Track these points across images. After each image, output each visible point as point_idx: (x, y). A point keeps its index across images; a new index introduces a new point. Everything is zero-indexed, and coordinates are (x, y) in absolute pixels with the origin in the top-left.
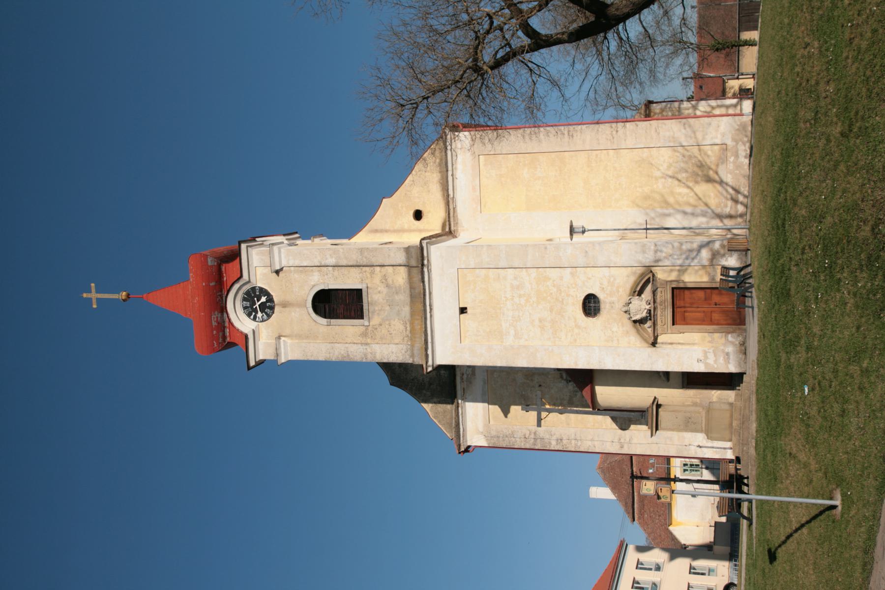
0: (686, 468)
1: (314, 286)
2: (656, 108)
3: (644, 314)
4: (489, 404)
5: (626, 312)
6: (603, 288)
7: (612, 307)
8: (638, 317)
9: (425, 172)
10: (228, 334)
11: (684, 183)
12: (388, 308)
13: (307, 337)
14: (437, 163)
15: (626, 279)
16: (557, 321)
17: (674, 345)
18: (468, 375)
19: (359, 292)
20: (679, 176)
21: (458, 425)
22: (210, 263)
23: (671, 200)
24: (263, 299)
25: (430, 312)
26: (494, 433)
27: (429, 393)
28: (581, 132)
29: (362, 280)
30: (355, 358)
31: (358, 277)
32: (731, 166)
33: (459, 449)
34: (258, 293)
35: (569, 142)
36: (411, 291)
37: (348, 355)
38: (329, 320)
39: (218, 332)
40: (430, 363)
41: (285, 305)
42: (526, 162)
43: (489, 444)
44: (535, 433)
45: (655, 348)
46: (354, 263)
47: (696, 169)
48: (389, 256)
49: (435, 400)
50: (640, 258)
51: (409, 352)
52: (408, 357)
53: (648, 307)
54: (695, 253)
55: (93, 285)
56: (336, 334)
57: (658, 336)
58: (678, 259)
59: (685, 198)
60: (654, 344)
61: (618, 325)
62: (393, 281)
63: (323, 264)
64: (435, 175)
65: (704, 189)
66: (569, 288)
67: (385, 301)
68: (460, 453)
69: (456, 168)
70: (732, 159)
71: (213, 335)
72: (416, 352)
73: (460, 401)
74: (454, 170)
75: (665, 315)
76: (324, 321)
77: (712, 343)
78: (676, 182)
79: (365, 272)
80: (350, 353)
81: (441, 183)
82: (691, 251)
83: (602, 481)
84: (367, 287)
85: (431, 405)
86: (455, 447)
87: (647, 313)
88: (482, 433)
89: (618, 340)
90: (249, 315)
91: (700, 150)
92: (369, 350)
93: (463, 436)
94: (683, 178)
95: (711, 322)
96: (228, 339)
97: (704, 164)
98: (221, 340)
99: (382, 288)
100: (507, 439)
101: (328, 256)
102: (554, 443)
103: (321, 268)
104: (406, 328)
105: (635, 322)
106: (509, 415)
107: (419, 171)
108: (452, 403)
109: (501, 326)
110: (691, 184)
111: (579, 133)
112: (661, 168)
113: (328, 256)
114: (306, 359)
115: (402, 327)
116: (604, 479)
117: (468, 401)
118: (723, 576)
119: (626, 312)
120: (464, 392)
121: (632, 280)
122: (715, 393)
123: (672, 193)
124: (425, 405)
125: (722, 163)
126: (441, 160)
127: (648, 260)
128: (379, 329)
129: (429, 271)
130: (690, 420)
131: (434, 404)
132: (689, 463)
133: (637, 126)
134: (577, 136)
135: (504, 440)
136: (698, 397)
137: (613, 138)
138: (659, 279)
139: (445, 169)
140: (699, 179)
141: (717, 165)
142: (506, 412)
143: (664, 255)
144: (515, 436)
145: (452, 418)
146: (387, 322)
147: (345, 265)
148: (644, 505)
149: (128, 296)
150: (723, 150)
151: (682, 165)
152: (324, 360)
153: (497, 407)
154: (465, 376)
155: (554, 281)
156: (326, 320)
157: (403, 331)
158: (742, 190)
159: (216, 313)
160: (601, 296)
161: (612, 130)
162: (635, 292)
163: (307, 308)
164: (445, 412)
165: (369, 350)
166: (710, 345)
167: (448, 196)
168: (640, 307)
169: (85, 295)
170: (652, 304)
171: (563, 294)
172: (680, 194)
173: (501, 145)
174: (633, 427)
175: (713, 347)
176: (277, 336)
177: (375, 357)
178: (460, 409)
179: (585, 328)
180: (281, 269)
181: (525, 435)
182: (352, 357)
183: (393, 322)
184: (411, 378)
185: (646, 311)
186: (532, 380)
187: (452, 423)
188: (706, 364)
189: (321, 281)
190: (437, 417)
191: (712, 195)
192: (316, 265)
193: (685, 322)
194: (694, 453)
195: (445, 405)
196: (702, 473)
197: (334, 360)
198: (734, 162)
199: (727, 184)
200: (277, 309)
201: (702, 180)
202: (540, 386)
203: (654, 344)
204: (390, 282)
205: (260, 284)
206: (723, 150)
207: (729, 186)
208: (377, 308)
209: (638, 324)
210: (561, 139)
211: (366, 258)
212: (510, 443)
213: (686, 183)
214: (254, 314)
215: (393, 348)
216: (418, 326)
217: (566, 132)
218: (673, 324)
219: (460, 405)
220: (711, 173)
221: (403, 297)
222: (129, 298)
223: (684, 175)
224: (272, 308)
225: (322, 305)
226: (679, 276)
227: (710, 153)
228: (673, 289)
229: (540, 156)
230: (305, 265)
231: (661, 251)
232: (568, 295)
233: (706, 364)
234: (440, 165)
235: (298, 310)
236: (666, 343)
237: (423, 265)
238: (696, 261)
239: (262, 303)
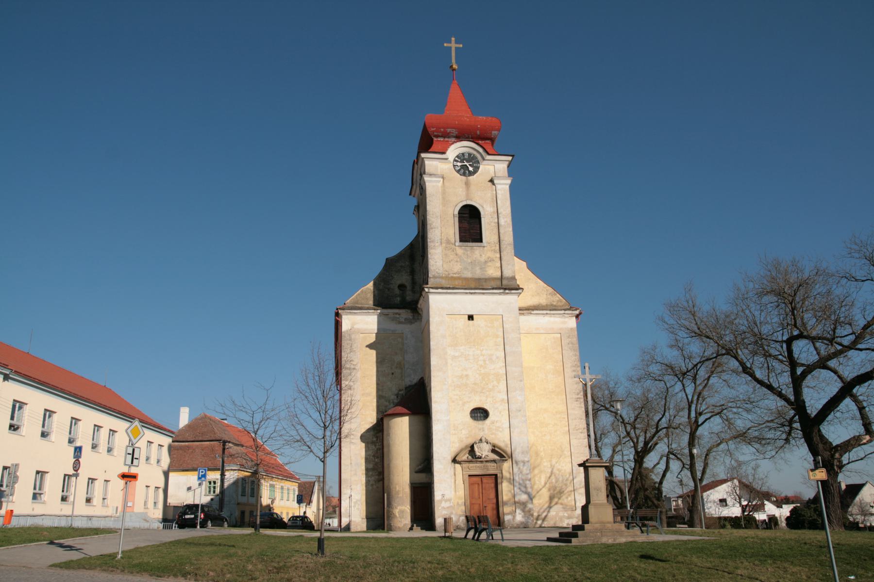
0: (212, 483)
1: (483, 207)
3: (478, 454)
4: (376, 334)
5: (481, 440)
6: (494, 423)
8: (476, 449)
10: (439, 139)
12: (469, 261)
13: (444, 198)
14: (553, 303)
15: (502, 439)
16: (467, 388)
17: (454, 476)
18: (398, 318)
19: (481, 241)
20: (553, 477)
21: (361, 309)
22: (493, 132)
23: (536, 471)
24: (471, 169)
26: (353, 336)
28: (580, 407)
32: (561, 514)
33: (340, 309)
34: (475, 165)
35: (573, 398)
36: (483, 279)
37: (432, 228)
38: (458, 216)
39: (442, 132)
40: (431, 290)
41: (467, 184)
42: (557, 368)
43: (344, 332)
47: (558, 489)
49: (376, 292)
50: (518, 450)
51: (437, 275)
52: (433, 274)
53: (483, 456)
54: (523, 489)
55: (445, 45)
57: (460, 464)
58: (519, 478)
59: (537, 482)
60: (454, 461)
63: (500, 215)
64: (544, 301)
65: (545, 495)
67: (474, 259)
70: (566, 515)
73: (379, 311)
75: (476, 469)
76: (456, 212)
79: (495, 246)
80: (433, 230)
81: (539, 305)
82: (526, 487)
83: (193, 418)
84: (484, 247)
85: (372, 288)
87: (479, 456)
89: (456, 434)
90: (457, 156)
91: (571, 491)
92: (437, 244)
93: (350, 313)
95: (472, 504)
96: (435, 139)
97: (562, 495)
98: (436, 133)
101: (505, 220)
103: (496, 214)
105: (472, 447)
106: (368, 349)
107: (547, 290)
108: (374, 305)
109: (461, 346)
110: (547, 486)
111: (579, 405)
113: (505, 220)
115: (455, 270)
116: (196, 419)
117: (378, 318)
118: (154, 514)
119: (481, 440)
121: (501, 444)
123: (541, 472)
126: (555, 306)
129: (500, 294)
131: (372, 291)
132: (216, 485)
134: (577, 404)
137: (577, 430)
140: (552, 492)
142: (370, 346)
143: (521, 468)
148: (178, 450)
149: (454, 70)
150: (572, 508)
151: (561, 479)
154: (398, 316)
155: (497, 386)
156: (457, 213)
158: (545, 523)
159: (457, 133)
160: (488, 421)
161: (582, 429)
162: (494, 446)
163: (466, 200)
164: (367, 299)
165: (437, 244)
166: (456, 504)
167: (533, 310)
168: (483, 451)
170: (486, 460)
171: (488, 393)
172: (540, 478)
174: (363, 445)
175: (454, 505)
176: (444, 176)
178: (373, 311)
179: (463, 409)
180: (494, 184)
183: (459, 264)
185: (481, 455)
187: (357, 304)
188: (441, 501)
190: (363, 293)
191: (541, 501)
192: (499, 210)
193: (471, 485)
195: (372, 299)
196: (208, 495)
198: (564, 516)
199: (549, 512)
200: (464, 178)
201: (551, 493)
203: (454, 461)
204: (490, 264)
205: (481, 167)
206: (572, 508)
208: (469, 252)
209: (470, 449)
211: (506, 247)
212: (346, 348)
213: (548, 482)
215: (440, 263)
217: (579, 396)
218: (469, 476)
219: (376, 311)
220: (556, 500)
221: (478, 273)
223: (554, 481)
224: (464, 174)
225: (467, 212)
226: (506, 479)
227: (569, 498)
230: (498, 202)
231: (524, 465)
233: (441, 501)
235: (464, 193)
236: (455, 470)
237: (505, 289)
239: (468, 167)
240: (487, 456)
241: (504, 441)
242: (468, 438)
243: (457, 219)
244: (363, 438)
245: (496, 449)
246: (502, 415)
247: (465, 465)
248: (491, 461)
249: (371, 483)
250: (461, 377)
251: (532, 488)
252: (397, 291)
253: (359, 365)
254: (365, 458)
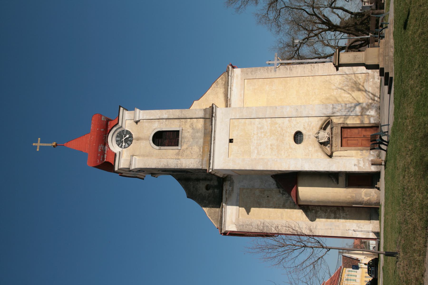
1: (155, 129)
2: (344, 217)
3: (326, 140)
4: (239, 207)
5: (316, 137)
6: (305, 128)
7: (309, 137)
9: (217, 88)
10: (106, 157)
11: (347, 92)
12: (192, 140)
13: (147, 156)
14: (223, 84)
15: (317, 123)
16: (280, 146)
17: (342, 157)
18: (229, 191)
19: (178, 132)
20: (344, 88)
22: (103, 119)
23: (340, 100)
24: (127, 136)
25: (214, 141)
26: (241, 223)
27: (207, 202)
29: (180, 126)
30: (171, 166)
31: (178, 124)
32: (371, 83)
33: (221, 231)
34: (125, 133)
36: (205, 131)
37: (168, 165)
40: (211, 167)
41: (138, 139)
42: (268, 83)
43: (238, 230)
44: (263, 223)
45: (331, 159)
46: (177, 117)
47: (353, 85)
48: (195, 113)
49: (210, 206)
50: (325, 112)
51: (200, 163)
52: (199, 165)
53: (328, 136)
54: (352, 109)
56: (163, 154)
57: (333, 152)
60: (331, 156)
61: (312, 147)
62: (196, 126)
63: (161, 118)
64: (222, 89)
66: (287, 128)
68: (221, 234)
69: (232, 86)
71: (98, 156)
72: (204, 162)
73: (224, 204)
74: (232, 86)
75: (337, 141)
76: (158, 148)
77: (362, 156)
78: (343, 91)
81: (224, 93)
82: (351, 107)
84: (182, 129)
85: (208, 208)
86: (219, 231)
87: (327, 139)
88: (234, 223)
89: (312, 155)
90: (118, 145)
91: (355, 76)
92: (179, 162)
94: (347, 89)
96: (105, 160)
98: (101, 160)
99: (190, 130)
100: (248, 227)
101: (164, 114)
102: (273, 229)
103: (160, 120)
104: (200, 151)
105: (321, 143)
106: (250, 213)
107: (214, 88)
109: (250, 148)
110: (350, 92)
111: (295, 69)
112: (336, 85)
113: (164, 114)
114: (145, 167)
115: (198, 150)
119: (316, 137)
120: (226, 200)
121: (320, 123)
122: (363, 190)
123: (340, 96)
124: (204, 209)
125: (367, 82)
126: (225, 82)
127: (329, 113)
128: (186, 151)
129: (215, 120)
130: (356, 57)
131: (209, 208)
133: (324, 65)
134: (294, 70)
135: (246, 227)
136: (354, 192)
137: (312, 71)
138: (334, 122)
139: (227, 86)
140: (355, 89)
141: (364, 83)
142: (248, 211)
144: (252, 225)
145: (219, 216)
146: (190, 148)
147: (172, 118)
149: (56, 145)
150: (367, 76)
151: (346, 83)
152: (155, 168)
153: (244, 208)
154: (228, 191)
155: (279, 125)
157: (198, 152)
158: (377, 95)
159: (102, 145)
160: (303, 132)
161: (312, 67)
162: (321, 128)
164: (215, 212)
165: (179, 162)
166: (362, 156)
167: (228, 98)
168: (324, 136)
169: (34, 144)
170: (331, 134)
171: (284, 131)
172: (345, 97)
173: (256, 74)
174: (317, 219)
176: (132, 155)
177: (182, 166)
179: (295, 149)
180: (139, 121)
181: (258, 224)
182: (170, 166)
183: (193, 147)
184: (199, 194)
185: (327, 138)
186: (264, 194)
187: (218, 219)
188: (359, 167)
189: (159, 127)
191: (361, 97)
192: (157, 118)
194: (351, 235)
197: (160, 167)
199: (369, 92)
200: (134, 141)
201: (356, 90)
202: (268, 197)
203: (331, 156)
205: (127, 129)
206: (367, 76)
207: (370, 93)
208: (186, 140)
210: (286, 71)
212: (249, 229)
214: (121, 144)
215: (192, 161)
216: (207, 149)
217: (289, 68)
218: (341, 146)
219: (224, 207)
220: (361, 87)
221: (200, 135)
222: (57, 145)
223: (347, 88)
224: (131, 141)
225: (157, 140)
226: (344, 120)
227: (360, 77)
228: (342, 128)
229: (275, 80)
230: (152, 118)
232: (286, 132)
233: (359, 167)
234: (225, 84)
236: (337, 156)
237: (212, 116)
238: (353, 112)
240: (328, 133)
241: (318, 121)
242: (314, 146)
243: (162, 147)
244: (313, 219)
245: (323, 127)
246: (300, 122)
247: (334, 149)
248: (331, 130)
249: (345, 215)
250: (272, 149)
251: (351, 103)
252: (210, 191)
253: (261, 220)
254: (326, 218)
